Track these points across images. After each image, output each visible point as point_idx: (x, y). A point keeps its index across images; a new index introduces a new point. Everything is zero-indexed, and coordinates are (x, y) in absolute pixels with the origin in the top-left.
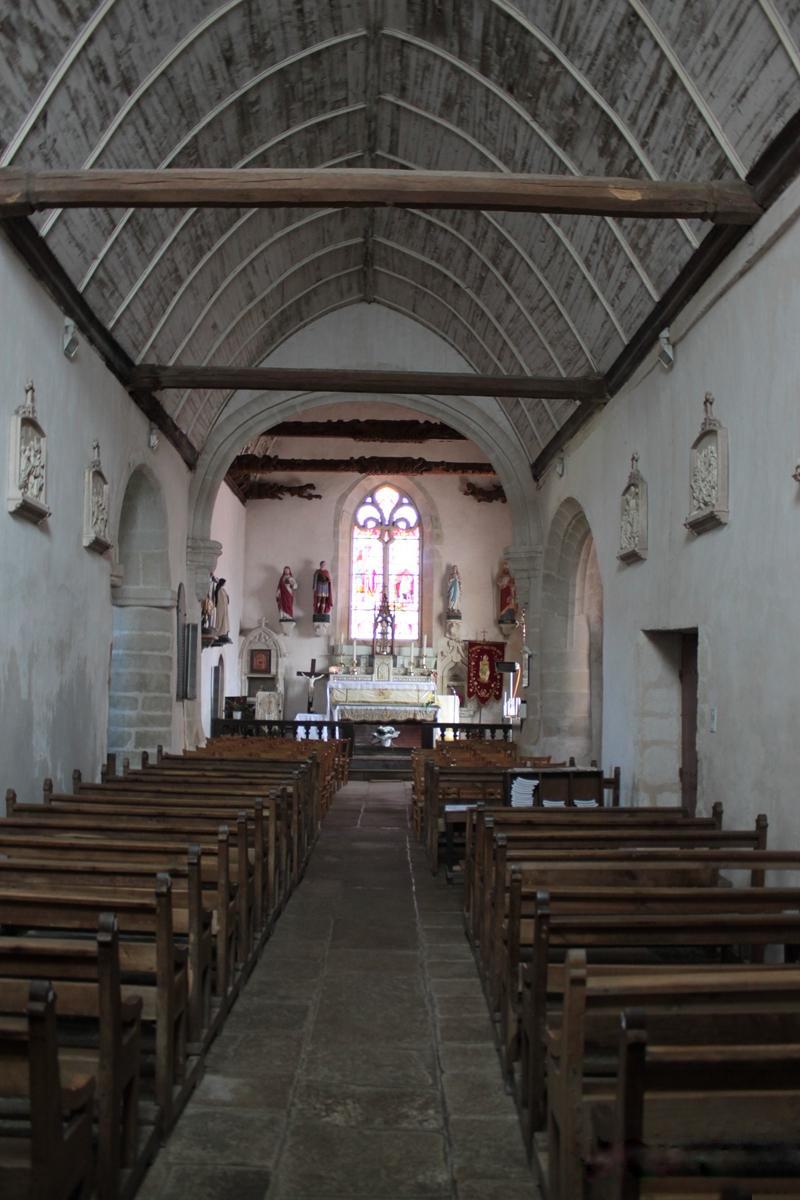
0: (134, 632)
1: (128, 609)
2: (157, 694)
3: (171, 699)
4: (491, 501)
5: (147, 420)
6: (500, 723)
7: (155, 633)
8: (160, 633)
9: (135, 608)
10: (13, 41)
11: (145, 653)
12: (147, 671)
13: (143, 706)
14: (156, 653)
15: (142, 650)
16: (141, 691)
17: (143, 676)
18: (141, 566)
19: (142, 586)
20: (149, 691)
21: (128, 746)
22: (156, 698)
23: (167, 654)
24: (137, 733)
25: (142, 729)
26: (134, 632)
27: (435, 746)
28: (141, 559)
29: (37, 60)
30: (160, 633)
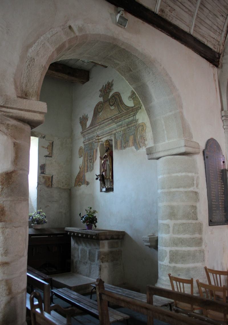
0: (165, 176)
1: (161, 160)
2: (184, 221)
3: (201, 224)
4: (97, 219)
5: (113, 6)
6: (130, 17)
7: (179, 174)
8: (184, 174)
9: (165, 158)
10: (140, 126)
11: (173, 190)
12: (174, 204)
13: (173, 230)
14: (182, 189)
15: (170, 188)
16: (171, 219)
17: (172, 208)
18: (164, 127)
19: (167, 141)
20: (177, 219)
21: (165, 261)
22: (183, 224)
23: (191, 189)
24: (170, 251)
25: (174, 249)
26: (165, 176)
27: (111, 94)
28: (163, 122)
29: (149, 112)
30: (184, 174)
